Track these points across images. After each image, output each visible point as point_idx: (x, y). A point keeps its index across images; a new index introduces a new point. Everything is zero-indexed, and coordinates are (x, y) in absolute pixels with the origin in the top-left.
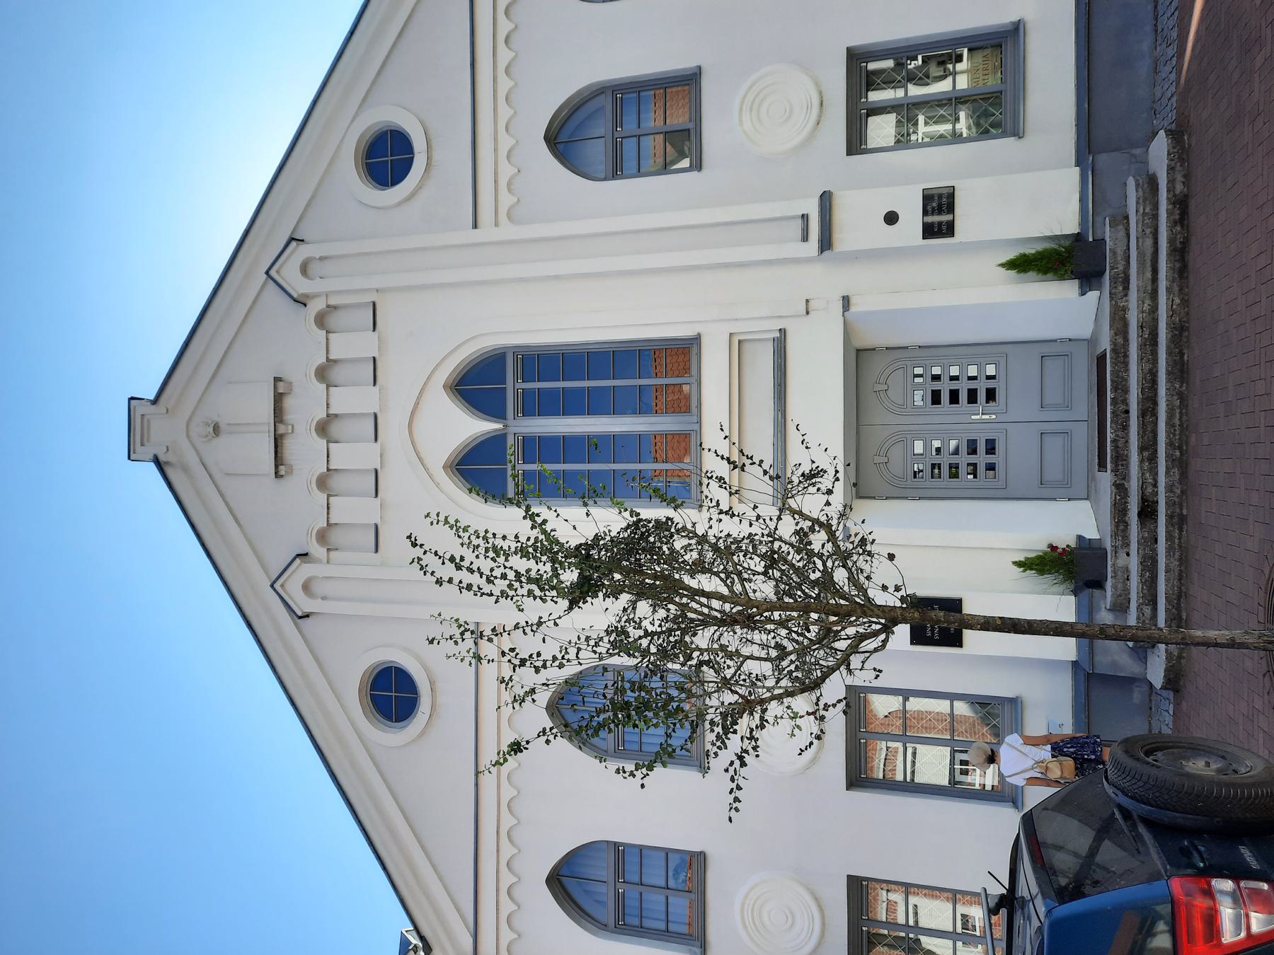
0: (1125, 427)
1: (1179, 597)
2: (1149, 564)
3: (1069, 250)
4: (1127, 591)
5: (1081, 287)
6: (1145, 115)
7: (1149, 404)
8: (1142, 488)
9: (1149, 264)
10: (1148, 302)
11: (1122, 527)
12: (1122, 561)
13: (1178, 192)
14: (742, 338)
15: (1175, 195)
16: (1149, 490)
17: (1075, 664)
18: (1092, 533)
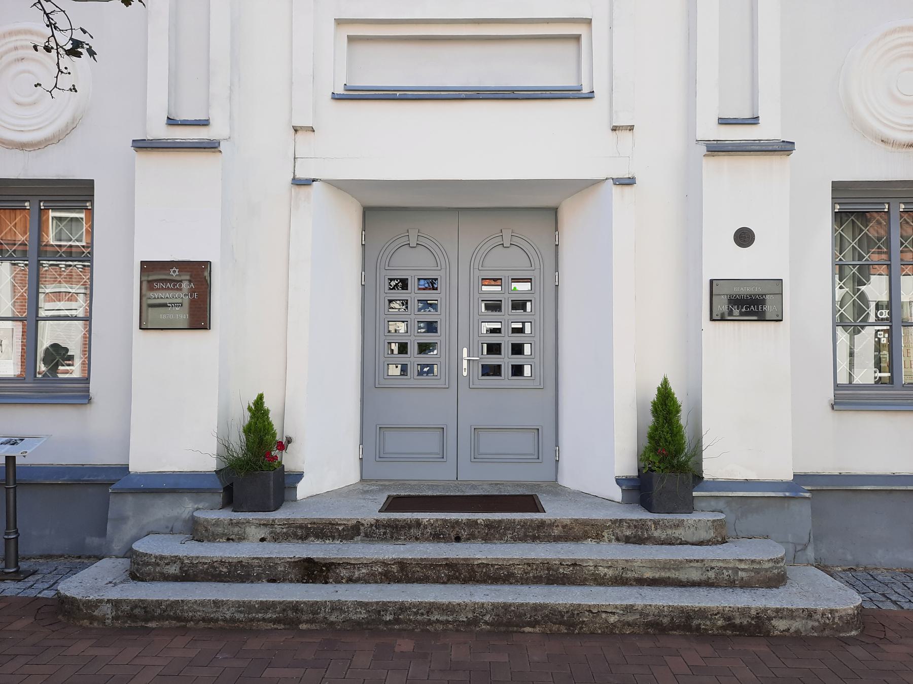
0: (437, 537)
1: (178, 619)
2: (239, 572)
3: (681, 468)
4: (213, 538)
5: (628, 479)
6: (849, 557)
7: (464, 574)
8: (346, 564)
9: (664, 574)
10: (610, 573)
11: (299, 532)
12: (254, 532)
13: (774, 622)
14: (584, 40)
15: (770, 619)
16: (344, 573)
17: (125, 469)
18: (303, 490)
